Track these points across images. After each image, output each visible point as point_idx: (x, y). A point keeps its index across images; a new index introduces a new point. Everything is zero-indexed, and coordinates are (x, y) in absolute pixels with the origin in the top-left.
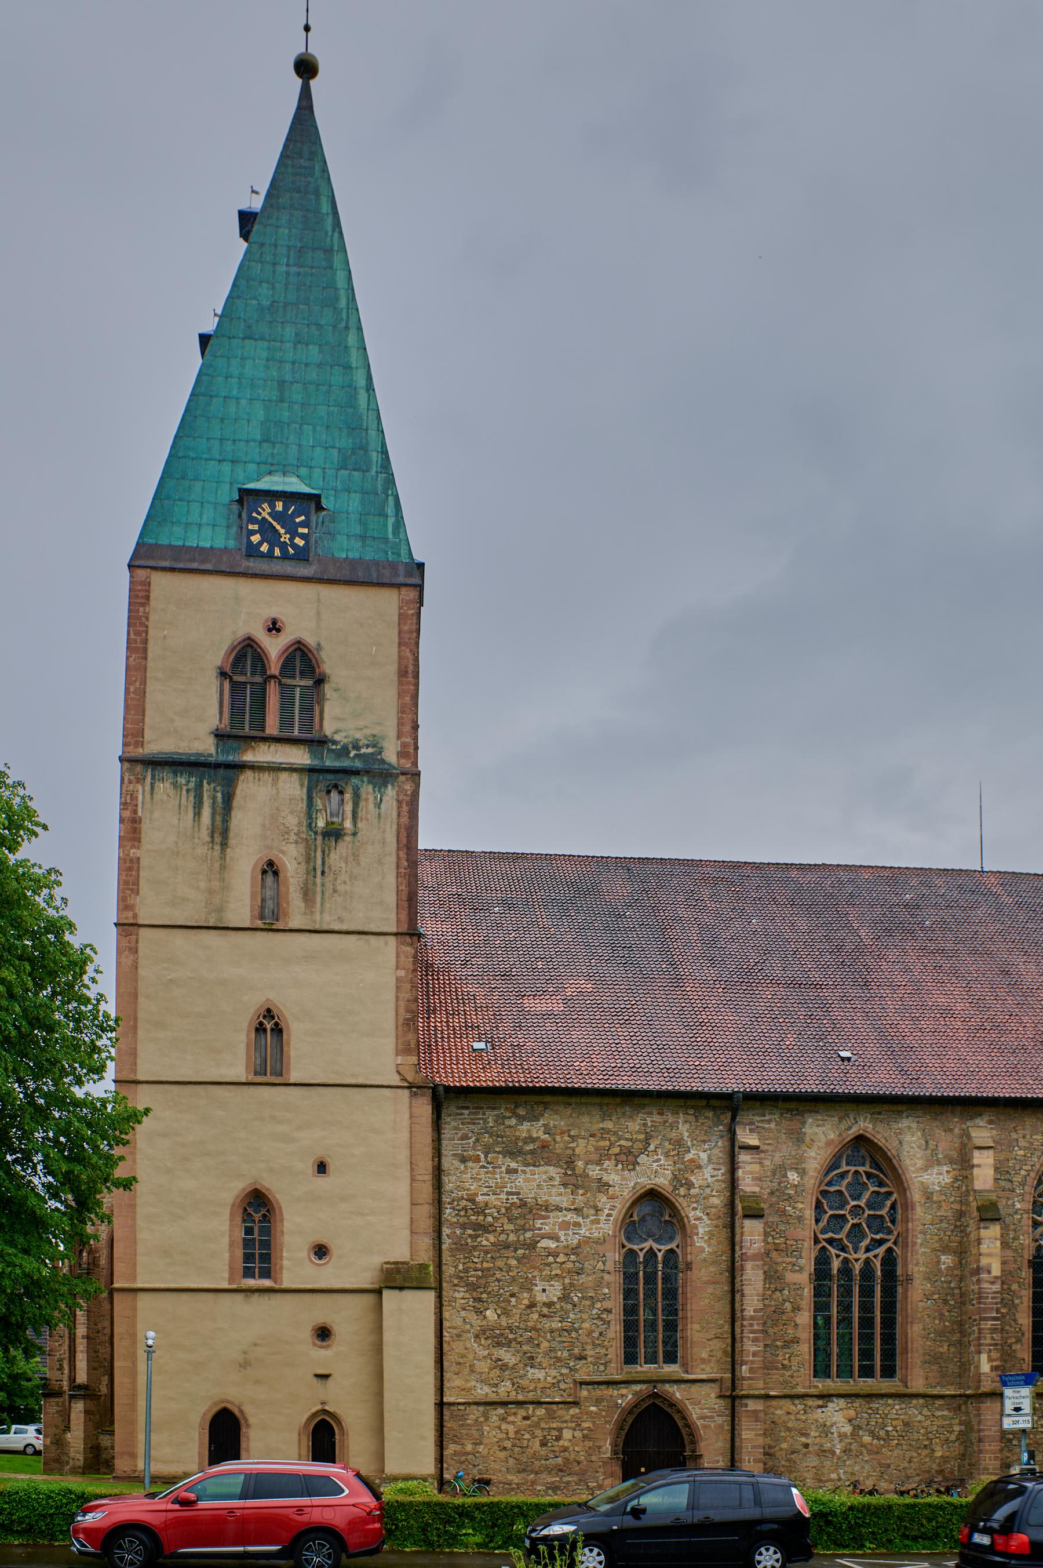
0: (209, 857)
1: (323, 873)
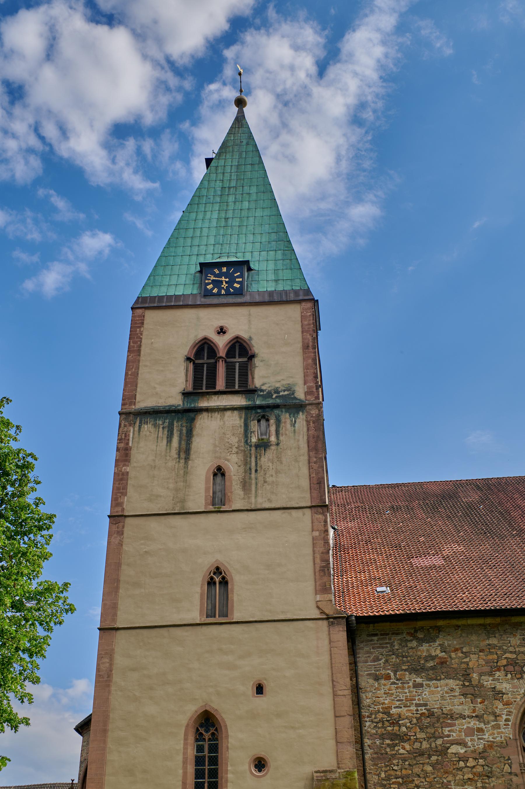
0: (176, 467)
1: (256, 471)
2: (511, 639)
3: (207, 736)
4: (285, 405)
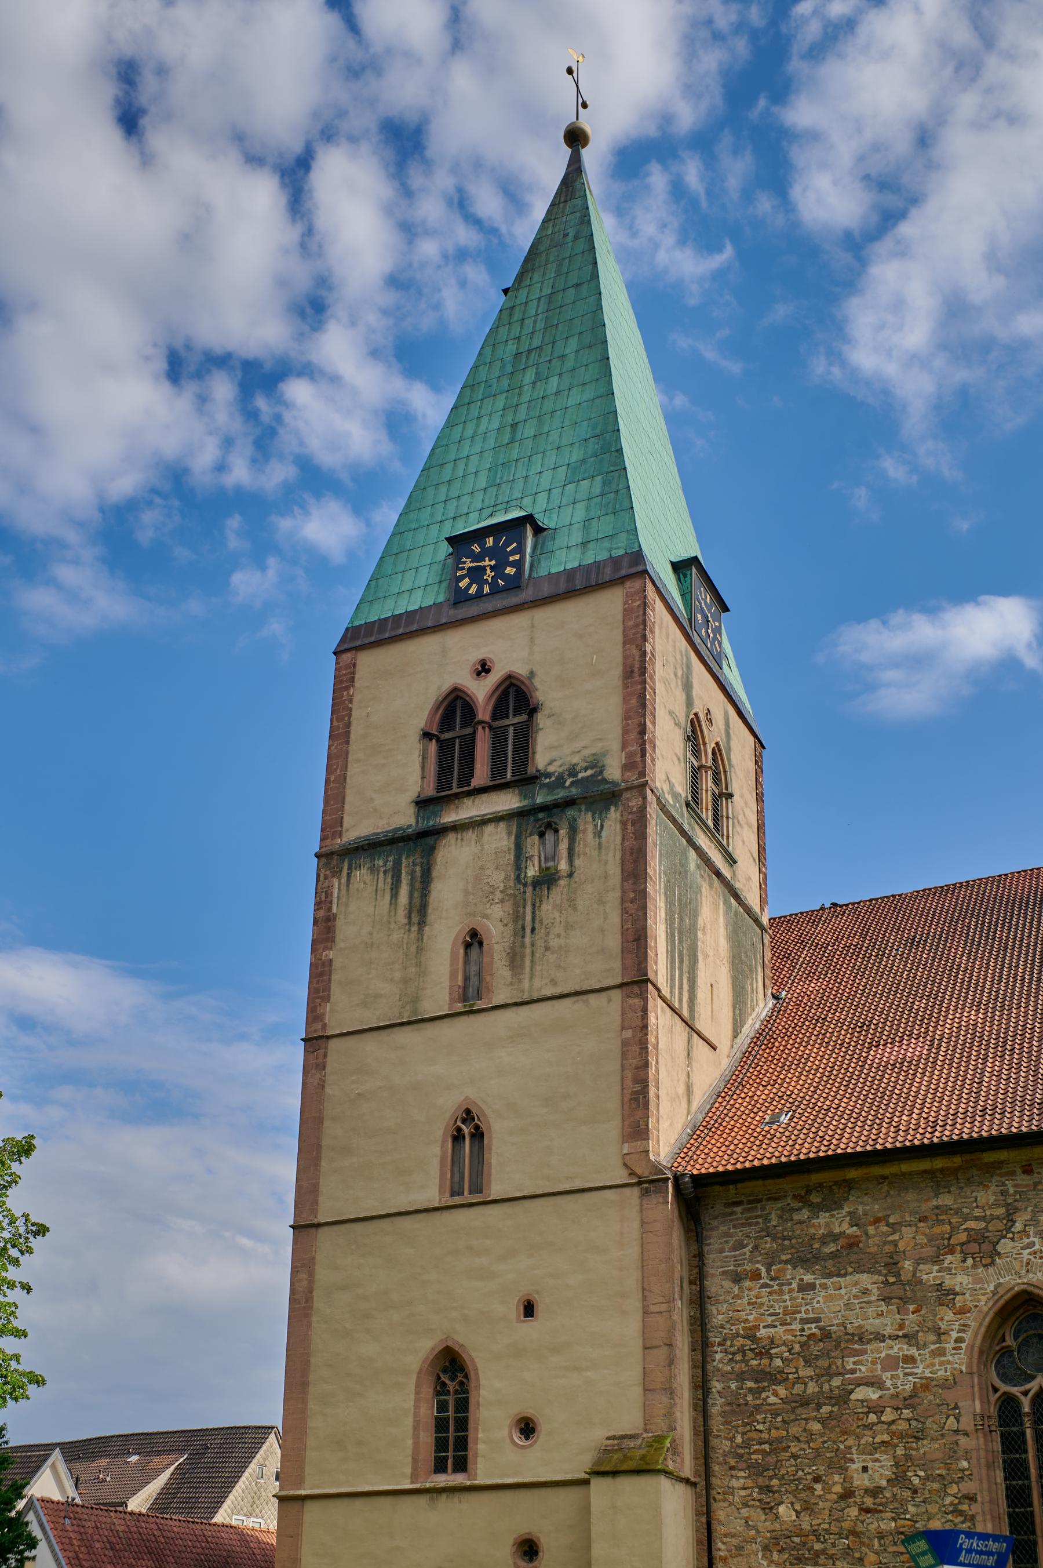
0: (405, 941)
1: (533, 930)
2: (979, 1195)
3: (451, 1386)
4: (585, 798)
